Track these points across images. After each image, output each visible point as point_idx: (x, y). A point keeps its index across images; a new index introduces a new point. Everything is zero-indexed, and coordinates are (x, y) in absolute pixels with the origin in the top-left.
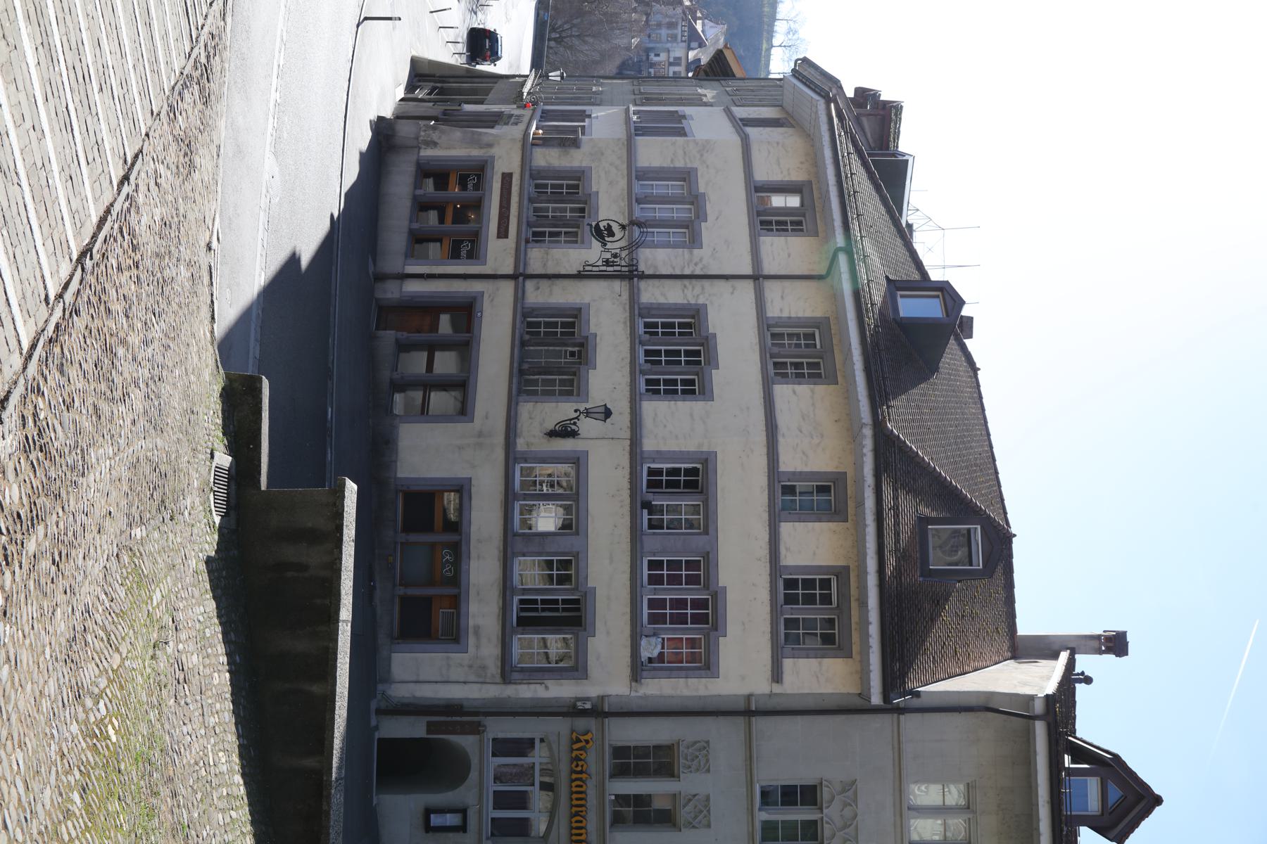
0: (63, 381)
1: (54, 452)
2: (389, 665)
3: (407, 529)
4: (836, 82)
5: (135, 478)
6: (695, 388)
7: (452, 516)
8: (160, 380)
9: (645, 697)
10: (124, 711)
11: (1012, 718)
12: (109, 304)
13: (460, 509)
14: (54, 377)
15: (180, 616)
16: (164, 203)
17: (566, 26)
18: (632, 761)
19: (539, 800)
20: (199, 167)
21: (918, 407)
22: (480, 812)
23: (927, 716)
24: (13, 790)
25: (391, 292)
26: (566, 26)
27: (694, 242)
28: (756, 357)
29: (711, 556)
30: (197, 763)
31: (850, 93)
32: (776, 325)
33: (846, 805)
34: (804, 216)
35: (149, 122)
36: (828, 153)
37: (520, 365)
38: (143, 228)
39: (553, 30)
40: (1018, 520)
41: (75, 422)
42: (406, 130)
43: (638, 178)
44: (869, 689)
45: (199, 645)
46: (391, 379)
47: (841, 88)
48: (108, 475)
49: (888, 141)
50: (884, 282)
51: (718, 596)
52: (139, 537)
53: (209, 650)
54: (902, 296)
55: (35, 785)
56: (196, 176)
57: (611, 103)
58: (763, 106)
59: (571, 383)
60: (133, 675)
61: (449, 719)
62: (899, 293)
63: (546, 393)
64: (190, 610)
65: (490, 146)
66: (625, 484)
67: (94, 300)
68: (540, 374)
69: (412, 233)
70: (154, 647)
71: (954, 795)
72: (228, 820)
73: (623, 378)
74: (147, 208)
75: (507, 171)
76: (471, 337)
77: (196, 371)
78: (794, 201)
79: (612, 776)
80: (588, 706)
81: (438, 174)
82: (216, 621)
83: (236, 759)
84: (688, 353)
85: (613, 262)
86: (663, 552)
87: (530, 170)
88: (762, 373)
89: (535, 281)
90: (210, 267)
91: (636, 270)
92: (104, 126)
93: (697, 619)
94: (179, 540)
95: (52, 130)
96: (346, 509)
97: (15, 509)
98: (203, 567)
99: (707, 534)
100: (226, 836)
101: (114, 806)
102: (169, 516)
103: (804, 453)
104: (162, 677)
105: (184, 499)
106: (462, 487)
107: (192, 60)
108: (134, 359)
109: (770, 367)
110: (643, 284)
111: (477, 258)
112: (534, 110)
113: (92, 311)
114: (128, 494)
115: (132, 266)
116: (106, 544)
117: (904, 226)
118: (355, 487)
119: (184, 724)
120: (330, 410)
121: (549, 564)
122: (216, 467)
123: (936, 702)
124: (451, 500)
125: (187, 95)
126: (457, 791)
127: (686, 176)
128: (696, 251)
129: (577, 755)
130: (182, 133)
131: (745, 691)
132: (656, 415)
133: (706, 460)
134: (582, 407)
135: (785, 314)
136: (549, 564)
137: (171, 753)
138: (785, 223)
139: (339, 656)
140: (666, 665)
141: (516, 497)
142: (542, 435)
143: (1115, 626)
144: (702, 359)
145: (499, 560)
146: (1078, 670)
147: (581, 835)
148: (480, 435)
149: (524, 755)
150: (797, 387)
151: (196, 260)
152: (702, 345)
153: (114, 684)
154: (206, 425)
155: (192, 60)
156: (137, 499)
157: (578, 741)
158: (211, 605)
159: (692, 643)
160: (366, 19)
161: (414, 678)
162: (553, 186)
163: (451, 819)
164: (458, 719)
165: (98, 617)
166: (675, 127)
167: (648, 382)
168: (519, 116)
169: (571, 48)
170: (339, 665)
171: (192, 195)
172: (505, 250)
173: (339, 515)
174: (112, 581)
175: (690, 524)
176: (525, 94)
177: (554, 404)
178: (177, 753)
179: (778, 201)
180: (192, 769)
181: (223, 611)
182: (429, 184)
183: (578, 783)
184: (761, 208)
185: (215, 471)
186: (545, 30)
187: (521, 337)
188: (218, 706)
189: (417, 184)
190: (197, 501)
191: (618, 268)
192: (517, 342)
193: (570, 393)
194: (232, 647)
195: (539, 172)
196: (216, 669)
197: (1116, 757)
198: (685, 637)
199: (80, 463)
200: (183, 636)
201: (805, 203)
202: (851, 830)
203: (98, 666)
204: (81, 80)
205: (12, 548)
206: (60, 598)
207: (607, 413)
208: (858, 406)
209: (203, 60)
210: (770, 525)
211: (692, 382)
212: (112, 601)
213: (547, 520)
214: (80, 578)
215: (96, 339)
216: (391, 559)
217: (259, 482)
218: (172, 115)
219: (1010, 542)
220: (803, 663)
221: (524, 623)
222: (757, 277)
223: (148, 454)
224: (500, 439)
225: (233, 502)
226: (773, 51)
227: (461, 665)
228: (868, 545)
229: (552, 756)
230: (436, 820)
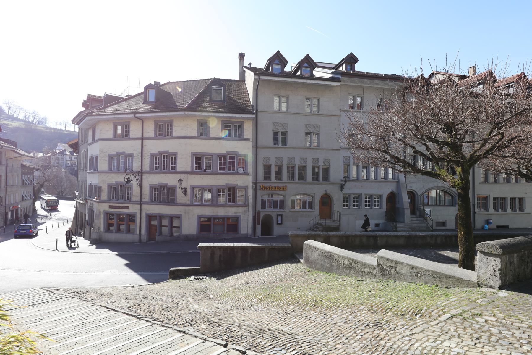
0: (173, 319)
1: (192, 319)
3: (210, 231)
4: (80, 113)
6: (174, 157)
7: (206, 219)
12: (151, 310)
14: (172, 321)
15: (232, 285)
16: (120, 300)
17: (58, 190)
19: (275, 198)
24: (273, 317)
25: (144, 238)
26: (58, 190)
28: (165, 140)
30: (267, 278)
31: (84, 109)
34: (124, 125)
35: (96, 306)
36: (104, 117)
38: (128, 304)
39: (59, 194)
40: (211, 76)
41: (184, 315)
42: (94, 236)
47: (82, 111)
49: (100, 99)
50: (144, 105)
51: (228, 153)
55: (272, 313)
56: (111, 292)
57: (87, 177)
58: (88, 134)
63: (174, 196)
65: (100, 212)
66: (199, 176)
67: (150, 314)
68: (169, 198)
69: (126, 233)
71: (276, 99)
73: (171, 176)
74: (122, 304)
78: (119, 128)
79: (271, 181)
80: (254, 186)
81: (108, 226)
82: (233, 276)
83: (266, 269)
84: (164, 158)
86: (217, 166)
87: (108, 200)
92: (99, 317)
95: (101, 330)
97: (207, 326)
98: (220, 281)
101: (276, 295)
107: (74, 297)
108: (166, 302)
109: (168, 137)
110: (144, 170)
111: (135, 215)
112: (88, 199)
113: (153, 314)
116: (215, 304)
117: (127, 97)
118: (200, 244)
121: (219, 195)
123: (255, 102)
124: (202, 220)
125: (86, 297)
126: (273, 217)
127: (111, 157)
128: (134, 155)
130: (98, 297)
131: (251, 148)
133: (193, 155)
134: (178, 187)
135: (153, 132)
136: (219, 195)
138: (126, 130)
141: (202, 203)
142: (186, 197)
143: (237, 55)
146: (248, 66)
148: (185, 213)
149: (265, 201)
150: (174, 130)
152: (162, 155)
155: (74, 297)
158: (229, 277)
159: (240, 160)
160: (57, 249)
161: (247, 228)
163: (280, 218)
165: (233, 304)
167: (172, 169)
168: (90, 204)
169: (65, 189)
173: (207, 247)
175: (210, 160)
179: (119, 132)
184: (121, 137)
187: (158, 202)
189: (112, 232)
191: (139, 176)
192: (160, 204)
193: (175, 190)
197: (269, 60)
200: (237, 283)
204: (84, 325)
205: (217, 325)
206: (229, 313)
207: (180, 180)
209: (74, 294)
211: (172, 158)
214: (224, 309)
218: (93, 300)
219: (216, 79)
220: (245, 133)
221: (234, 202)
222: (142, 139)
224: (187, 208)
225: (203, 275)
226: (67, 129)
227: (244, 217)
229: (266, 195)
230: (280, 222)
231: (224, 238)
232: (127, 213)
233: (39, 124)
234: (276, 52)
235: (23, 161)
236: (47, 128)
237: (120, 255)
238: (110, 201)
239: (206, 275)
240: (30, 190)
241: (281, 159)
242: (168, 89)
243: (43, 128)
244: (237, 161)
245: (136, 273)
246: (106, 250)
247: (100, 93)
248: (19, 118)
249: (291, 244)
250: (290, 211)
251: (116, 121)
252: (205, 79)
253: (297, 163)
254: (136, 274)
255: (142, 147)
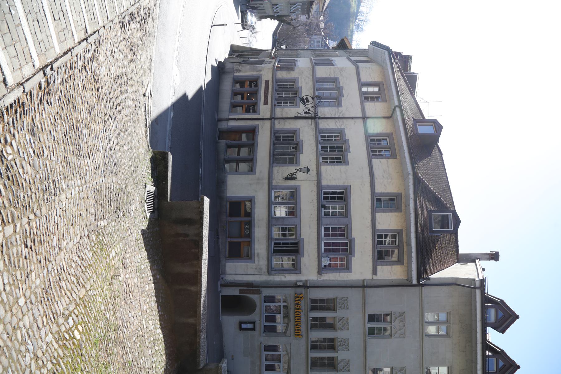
2: (225, 268)
3: (231, 216)
5: (99, 196)
7: (248, 210)
8: (114, 149)
9: (323, 280)
10: (87, 320)
11: (465, 288)
13: (251, 209)
18: (318, 305)
20: (139, 59)
21: (426, 168)
22: (260, 323)
23: (433, 287)
25: (224, 125)
27: (339, 105)
29: (349, 225)
30: (137, 329)
32: (372, 136)
33: (401, 321)
34: (381, 95)
37: (273, 152)
39: (278, 43)
42: (229, 66)
43: (317, 82)
44: (412, 278)
45: (138, 273)
46: (224, 158)
48: (78, 195)
49: (407, 69)
50: (412, 119)
52: (102, 225)
53: (143, 275)
54: (419, 125)
59: (293, 159)
60: (93, 298)
61: (248, 288)
62: (418, 124)
63: (283, 163)
64: (133, 257)
65: (260, 71)
66: (315, 198)
68: (281, 156)
69: (231, 103)
70: (111, 279)
71: (443, 317)
72: (154, 351)
73: (313, 157)
75: (267, 80)
76: (254, 142)
77: (137, 148)
78: (376, 89)
80: (301, 284)
81: (241, 82)
82: (147, 261)
83: (158, 322)
84: (338, 147)
85: (308, 112)
86: (330, 225)
88: (367, 154)
89: (278, 120)
90: (145, 104)
91: (317, 115)
93: (343, 250)
94: (127, 225)
96: (204, 210)
98: (140, 237)
99: (347, 217)
100: (153, 359)
102: (122, 214)
103: (385, 185)
104: (116, 293)
105: (131, 206)
106: (252, 199)
109: (370, 152)
110: (320, 121)
111: (256, 112)
114: (94, 204)
115: (94, 89)
118: (209, 200)
119: (130, 312)
120: (201, 170)
122: (148, 191)
123: (436, 282)
127: (335, 80)
128: (340, 108)
129: (297, 303)
131: (362, 278)
132: (327, 171)
133: (347, 188)
137: (122, 328)
138: (373, 98)
139: (202, 275)
140: (331, 268)
142: (282, 179)
143: (494, 250)
144: (344, 149)
145: (266, 228)
147: (299, 332)
148: (258, 179)
150: (381, 160)
151: (137, 98)
153: (80, 306)
154: (143, 173)
156: (100, 207)
157: (298, 297)
158: (145, 253)
159: (341, 260)
160: (214, 25)
161: (234, 273)
162: (284, 85)
163: (250, 326)
164: (251, 288)
166: (330, 64)
167: (323, 158)
168: (271, 61)
170: (202, 279)
171: (136, 70)
172: (267, 109)
173: (201, 213)
174: (83, 249)
175: (341, 214)
176: (272, 54)
177: (287, 167)
178: (125, 327)
180: (134, 333)
181: (151, 256)
182: (238, 86)
183: (298, 313)
185: (147, 193)
186: (276, 43)
187: (274, 141)
188: (148, 300)
189: (233, 86)
190: (138, 207)
191: (310, 115)
192: (272, 144)
193: (293, 163)
194: (155, 272)
195: (279, 80)
196: (147, 283)
197: (502, 301)
198: (338, 257)
199: (52, 187)
200: (129, 271)
201: (381, 90)
202: (403, 331)
203: (69, 298)
207: (308, 170)
208: (407, 167)
210: (372, 214)
211: (340, 158)
212: (83, 260)
213: (281, 212)
215: (65, 121)
216: (225, 227)
217: (167, 198)
218: (123, 29)
221: (276, 251)
223: (107, 185)
224: (266, 181)
225: (156, 207)
227: (252, 268)
228: (411, 221)
230: (243, 326)
231: (220, 237)
232: (258, 102)
233: (355, 25)
234: (517, 314)
235: (317, 4)
236: (352, 32)
237: (200, 91)
238: (275, 82)
239: (156, 212)
240: (285, 12)
241: (346, 328)
242: (435, 151)
243: (351, 28)
244: (340, 255)
245: (171, 105)
246: (209, 77)
247: (414, 68)
248: (361, 7)
249: (203, 367)
250: (261, 343)
251: (385, 85)
252: (453, 203)
253: (340, 355)
254: (170, 105)
255: (352, 118)
